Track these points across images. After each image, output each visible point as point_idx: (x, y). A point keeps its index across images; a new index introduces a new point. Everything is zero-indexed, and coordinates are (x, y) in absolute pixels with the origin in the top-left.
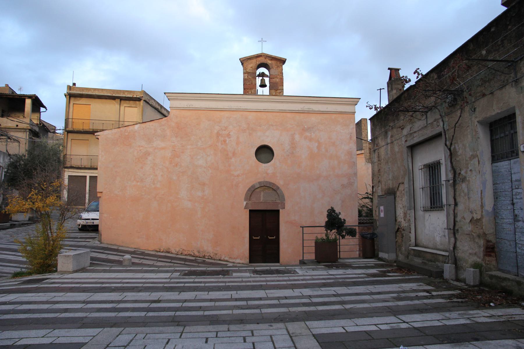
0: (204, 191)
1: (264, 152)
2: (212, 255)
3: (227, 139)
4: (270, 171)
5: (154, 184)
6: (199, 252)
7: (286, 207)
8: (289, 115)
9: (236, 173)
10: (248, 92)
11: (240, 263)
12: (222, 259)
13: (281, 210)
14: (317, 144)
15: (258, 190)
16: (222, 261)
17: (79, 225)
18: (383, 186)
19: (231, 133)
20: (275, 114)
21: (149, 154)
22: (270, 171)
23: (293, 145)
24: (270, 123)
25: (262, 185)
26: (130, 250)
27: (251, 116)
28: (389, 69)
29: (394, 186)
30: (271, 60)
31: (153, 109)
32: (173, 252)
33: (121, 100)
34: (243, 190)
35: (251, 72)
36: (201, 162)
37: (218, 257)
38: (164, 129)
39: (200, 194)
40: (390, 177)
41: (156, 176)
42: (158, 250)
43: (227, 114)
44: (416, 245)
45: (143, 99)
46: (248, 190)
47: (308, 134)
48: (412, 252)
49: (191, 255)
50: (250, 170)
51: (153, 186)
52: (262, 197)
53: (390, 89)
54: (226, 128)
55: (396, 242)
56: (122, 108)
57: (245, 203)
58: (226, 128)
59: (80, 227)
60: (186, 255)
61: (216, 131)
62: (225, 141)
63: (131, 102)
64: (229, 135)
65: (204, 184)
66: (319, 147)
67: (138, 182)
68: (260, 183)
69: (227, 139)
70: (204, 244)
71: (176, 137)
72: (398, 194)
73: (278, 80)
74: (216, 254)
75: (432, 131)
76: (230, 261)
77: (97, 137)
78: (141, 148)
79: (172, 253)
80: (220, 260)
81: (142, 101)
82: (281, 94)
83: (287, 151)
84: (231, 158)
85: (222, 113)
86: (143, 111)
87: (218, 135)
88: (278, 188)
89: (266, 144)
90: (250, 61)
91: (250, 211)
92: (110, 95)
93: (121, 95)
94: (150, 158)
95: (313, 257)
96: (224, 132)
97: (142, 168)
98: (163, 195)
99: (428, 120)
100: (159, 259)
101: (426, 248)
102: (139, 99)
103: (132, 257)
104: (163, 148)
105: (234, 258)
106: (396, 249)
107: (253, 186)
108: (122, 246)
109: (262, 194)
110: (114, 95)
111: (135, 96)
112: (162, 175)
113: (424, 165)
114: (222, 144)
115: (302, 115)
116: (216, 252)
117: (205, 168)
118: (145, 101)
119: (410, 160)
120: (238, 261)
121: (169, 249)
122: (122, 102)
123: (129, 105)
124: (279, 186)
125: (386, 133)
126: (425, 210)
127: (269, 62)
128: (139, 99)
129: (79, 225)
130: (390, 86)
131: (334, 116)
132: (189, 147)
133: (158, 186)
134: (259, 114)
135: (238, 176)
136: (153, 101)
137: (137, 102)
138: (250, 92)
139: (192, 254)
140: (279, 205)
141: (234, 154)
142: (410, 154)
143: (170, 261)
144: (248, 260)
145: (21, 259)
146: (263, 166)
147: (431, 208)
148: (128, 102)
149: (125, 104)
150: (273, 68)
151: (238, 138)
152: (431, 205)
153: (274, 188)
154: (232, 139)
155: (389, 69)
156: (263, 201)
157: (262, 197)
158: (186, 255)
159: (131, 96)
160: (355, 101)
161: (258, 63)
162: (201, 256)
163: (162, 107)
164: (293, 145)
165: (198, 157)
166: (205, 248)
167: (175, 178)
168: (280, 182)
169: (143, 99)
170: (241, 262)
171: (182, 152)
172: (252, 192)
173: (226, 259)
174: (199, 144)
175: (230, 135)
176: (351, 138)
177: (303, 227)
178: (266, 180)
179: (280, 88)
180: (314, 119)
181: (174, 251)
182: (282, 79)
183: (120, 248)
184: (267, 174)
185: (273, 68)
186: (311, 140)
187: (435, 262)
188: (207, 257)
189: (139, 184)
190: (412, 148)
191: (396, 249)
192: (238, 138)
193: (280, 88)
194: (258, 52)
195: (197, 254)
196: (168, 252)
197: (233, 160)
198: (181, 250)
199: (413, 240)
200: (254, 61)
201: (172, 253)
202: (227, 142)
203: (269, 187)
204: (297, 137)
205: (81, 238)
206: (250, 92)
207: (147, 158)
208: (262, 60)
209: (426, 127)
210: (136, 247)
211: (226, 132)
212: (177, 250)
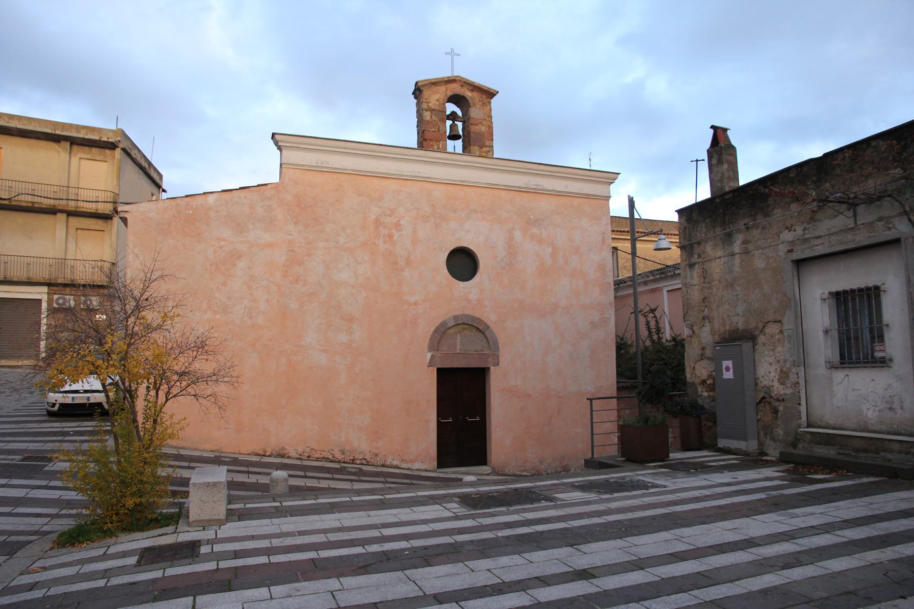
0: (351, 333)
1: (463, 263)
2: (368, 457)
3: (394, 231)
4: (473, 296)
5: (250, 318)
6: (343, 452)
7: (500, 364)
8: (504, 194)
9: (412, 299)
10: (432, 146)
11: (420, 470)
12: (388, 463)
13: (492, 368)
14: (550, 250)
15: (451, 331)
16: (387, 467)
17: (54, 405)
18: (716, 325)
19: (402, 222)
20: (479, 190)
21: (240, 257)
22: (473, 296)
23: (512, 250)
24: (472, 207)
25: (460, 322)
26: (205, 454)
27: (439, 192)
28: (712, 127)
29: (753, 325)
30: (472, 91)
31: (137, 169)
32: (291, 455)
33: (72, 144)
34: (425, 329)
35: (438, 108)
36: (345, 276)
37: (379, 460)
38: (269, 207)
39: (343, 338)
40: (740, 310)
41: (255, 301)
42: (261, 452)
43: (393, 185)
44: (809, 426)
45: (121, 146)
46: (435, 331)
47: (535, 231)
48: (808, 436)
49: (326, 459)
50: (437, 297)
51: (249, 322)
52: (458, 344)
53: (714, 162)
54: (393, 212)
55: (758, 420)
56: (75, 161)
57: (429, 355)
58: (393, 212)
59: (56, 408)
60: (317, 459)
61: (373, 217)
62: (391, 236)
63: (94, 149)
64: (398, 226)
65: (351, 319)
66: (553, 255)
67: (216, 312)
68: (455, 317)
69: (394, 231)
70: (354, 438)
71: (296, 223)
72: (761, 339)
73: (483, 129)
74: (376, 455)
75: (869, 237)
76: (403, 466)
77: (122, 215)
78: (222, 243)
79: (289, 457)
80: (383, 466)
81: (118, 151)
82: (490, 155)
83: (502, 260)
84: (403, 270)
85: (384, 183)
86: (119, 169)
87: (378, 223)
88: (488, 327)
89: (465, 245)
90: (434, 89)
91: (439, 370)
92: (49, 131)
93: (74, 134)
94: (241, 264)
95: (613, 451)
96: (388, 219)
97: (224, 284)
98: (270, 340)
99: (858, 218)
100: (251, 469)
101: (844, 429)
102: (112, 146)
103: (290, 476)
104: (270, 246)
105: (411, 461)
106: (758, 433)
107: (443, 324)
108: (183, 448)
109: (459, 338)
110: (58, 132)
111: (105, 139)
112: (267, 301)
113: (830, 293)
114: (385, 242)
115: (525, 195)
116: (376, 452)
117: (353, 286)
118: (124, 150)
119: (796, 283)
120: (417, 465)
121: (283, 448)
122: (75, 148)
123: (89, 157)
124: (488, 323)
125: (729, 236)
126: (832, 366)
127: (468, 94)
128: (112, 146)
129: (54, 405)
130: (716, 157)
131: (576, 202)
132: (321, 244)
133: (260, 321)
134: (452, 188)
135: (416, 304)
136: (136, 152)
137: (107, 151)
138: (436, 147)
139: (330, 457)
140: (490, 359)
141: (408, 261)
142: (795, 274)
143: (302, 473)
144: (435, 464)
145: (72, 495)
146: (462, 286)
147: (841, 363)
148: (86, 149)
149: (80, 153)
150: (475, 105)
151: (415, 231)
152: (841, 359)
153: (481, 327)
154: (404, 233)
155: (712, 127)
156: (461, 355)
157: (458, 344)
158: (317, 459)
159: (97, 138)
160: (610, 178)
161: (450, 93)
162: (347, 459)
163: (150, 164)
164: (512, 250)
165: (340, 266)
166: (356, 444)
167: (294, 305)
168: (490, 317)
169: (121, 146)
170: (423, 467)
171: (309, 255)
172: (441, 334)
173: (395, 463)
174: (342, 240)
175: (400, 225)
176: (603, 241)
177: (591, 400)
178: (468, 312)
179: (487, 143)
180: (545, 204)
181: (293, 454)
182: (490, 128)
183: (183, 452)
184: (469, 301)
185: (475, 105)
186: (540, 241)
187: (878, 453)
188: (358, 462)
189: (218, 316)
190: (799, 263)
191: (758, 433)
192: (415, 231)
193: (487, 143)
194: (446, 73)
195: (339, 456)
196: (283, 456)
197: (406, 273)
198: (308, 450)
199: (804, 418)
200: (442, 88)
201: (289, 457)
202: (395, 238)
203: (472, 326)
204: (518, 234)
205: (77, 433)
206: (436, 147)
207: (235, 265)
208: (455, 89)
209: (852, 229)
210: (214, 448)
211: (393, 220)
212: (300, 450)
